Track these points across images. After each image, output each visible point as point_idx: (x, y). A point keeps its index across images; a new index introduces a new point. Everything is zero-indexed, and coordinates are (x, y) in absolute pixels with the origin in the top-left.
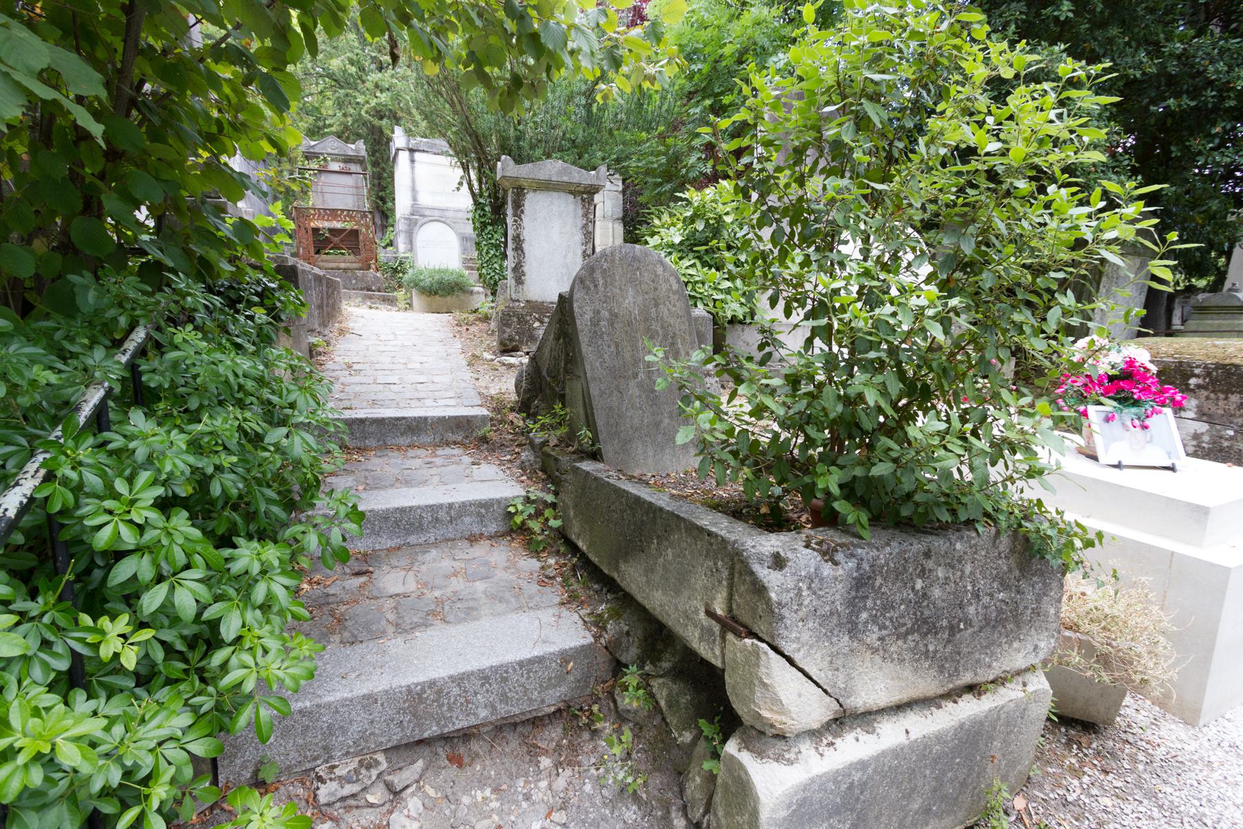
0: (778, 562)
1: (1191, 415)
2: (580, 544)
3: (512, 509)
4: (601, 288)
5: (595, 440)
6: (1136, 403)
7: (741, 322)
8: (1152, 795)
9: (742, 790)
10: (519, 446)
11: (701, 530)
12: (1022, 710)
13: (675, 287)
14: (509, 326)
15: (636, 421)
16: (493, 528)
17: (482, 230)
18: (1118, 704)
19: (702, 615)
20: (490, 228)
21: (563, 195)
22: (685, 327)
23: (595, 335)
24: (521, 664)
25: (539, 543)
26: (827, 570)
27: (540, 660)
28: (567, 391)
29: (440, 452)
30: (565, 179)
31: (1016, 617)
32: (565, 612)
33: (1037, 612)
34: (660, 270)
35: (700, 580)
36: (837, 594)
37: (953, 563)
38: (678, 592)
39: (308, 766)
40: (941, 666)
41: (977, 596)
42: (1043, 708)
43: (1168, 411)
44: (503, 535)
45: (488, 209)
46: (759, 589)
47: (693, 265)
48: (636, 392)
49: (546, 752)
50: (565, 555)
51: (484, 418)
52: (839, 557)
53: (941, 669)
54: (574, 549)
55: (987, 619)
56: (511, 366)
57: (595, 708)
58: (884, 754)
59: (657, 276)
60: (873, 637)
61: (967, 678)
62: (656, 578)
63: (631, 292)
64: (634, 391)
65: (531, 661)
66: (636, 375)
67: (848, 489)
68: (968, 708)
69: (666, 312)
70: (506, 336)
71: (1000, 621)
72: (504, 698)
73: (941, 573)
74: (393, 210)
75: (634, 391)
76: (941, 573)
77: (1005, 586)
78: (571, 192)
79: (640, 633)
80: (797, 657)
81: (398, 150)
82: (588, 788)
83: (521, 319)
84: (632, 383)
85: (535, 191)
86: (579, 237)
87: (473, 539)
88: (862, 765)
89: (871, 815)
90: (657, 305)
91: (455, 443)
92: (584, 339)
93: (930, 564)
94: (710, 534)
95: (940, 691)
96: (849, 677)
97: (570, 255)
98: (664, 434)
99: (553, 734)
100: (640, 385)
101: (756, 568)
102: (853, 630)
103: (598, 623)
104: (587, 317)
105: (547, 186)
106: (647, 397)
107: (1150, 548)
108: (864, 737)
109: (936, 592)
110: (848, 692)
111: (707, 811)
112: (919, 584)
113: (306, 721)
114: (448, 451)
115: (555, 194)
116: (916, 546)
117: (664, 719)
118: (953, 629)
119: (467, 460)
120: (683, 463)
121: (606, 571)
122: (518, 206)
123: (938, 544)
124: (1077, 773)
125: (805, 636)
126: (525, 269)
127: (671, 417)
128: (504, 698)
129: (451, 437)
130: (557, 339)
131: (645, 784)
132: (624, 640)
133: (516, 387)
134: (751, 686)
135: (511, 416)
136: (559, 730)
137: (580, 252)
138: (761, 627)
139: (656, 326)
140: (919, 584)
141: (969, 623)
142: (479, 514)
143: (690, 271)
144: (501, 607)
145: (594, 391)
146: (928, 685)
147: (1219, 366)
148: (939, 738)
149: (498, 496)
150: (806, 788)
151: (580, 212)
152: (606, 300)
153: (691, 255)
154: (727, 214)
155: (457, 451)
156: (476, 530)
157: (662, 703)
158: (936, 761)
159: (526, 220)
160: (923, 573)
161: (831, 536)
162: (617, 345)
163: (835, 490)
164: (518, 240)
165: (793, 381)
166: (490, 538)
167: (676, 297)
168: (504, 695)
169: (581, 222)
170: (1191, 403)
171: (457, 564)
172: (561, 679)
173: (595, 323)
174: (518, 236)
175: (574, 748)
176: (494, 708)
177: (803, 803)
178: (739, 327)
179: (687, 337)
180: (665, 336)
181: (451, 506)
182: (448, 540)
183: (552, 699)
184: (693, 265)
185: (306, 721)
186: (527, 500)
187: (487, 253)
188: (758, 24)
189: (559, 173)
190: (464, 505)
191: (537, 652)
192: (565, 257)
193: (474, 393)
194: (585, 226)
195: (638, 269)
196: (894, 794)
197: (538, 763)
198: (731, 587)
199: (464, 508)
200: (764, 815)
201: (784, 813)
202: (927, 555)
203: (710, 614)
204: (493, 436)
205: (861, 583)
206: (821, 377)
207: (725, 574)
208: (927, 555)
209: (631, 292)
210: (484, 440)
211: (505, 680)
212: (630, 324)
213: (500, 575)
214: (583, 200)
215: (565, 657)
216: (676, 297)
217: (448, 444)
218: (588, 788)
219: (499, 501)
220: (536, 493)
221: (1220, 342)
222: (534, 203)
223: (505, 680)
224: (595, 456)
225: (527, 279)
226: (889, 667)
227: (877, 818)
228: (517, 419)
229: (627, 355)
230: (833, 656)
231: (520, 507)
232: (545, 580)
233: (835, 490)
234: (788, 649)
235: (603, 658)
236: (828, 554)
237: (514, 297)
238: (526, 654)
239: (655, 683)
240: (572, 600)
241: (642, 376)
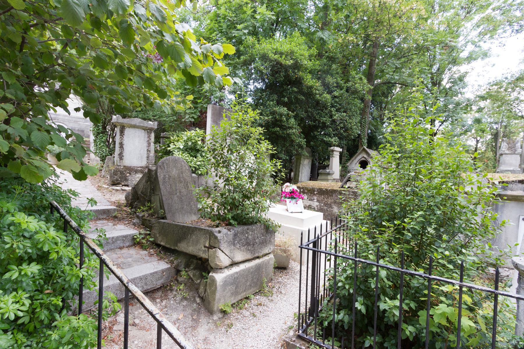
0: (219, 232)
1: (315, 201)
2: (162, 243)
3: (135, 237)
4: (166, 169)
5: (165, 213)
6: (295, 198)
8: (293, 278)
9: (213, 280)
10: (130, 218)
11: (202, 229)
12: (268, 261)
13: (187, 168)
14: (116, 175)
15: (176, 207)
16: (128, 244)
17: (97, 135)
18: (289, 262)
19: (203, 248)
20: (101, 135)
21: (140, 130)
22: (190, 180)
23: (164, 182)
24: (151, 274)
25: (146, 246)
26: (229, 233)
27: (156, 272)
28: (152, 199)
29: (98, 222)
30: (142, 125)
31: (266, 242)
32: (160, 262)
33: (270, 241)
34: (183, 163)
35: (202, 240)
36: (231, 237)
37: (253, 231)
38: (196, 245)
39: (89, 309)
40: (252, 252)
41: (258, 238)
42: (272, 262)
43: (301, 200)
44: (131, 246)
45: (101, 127)
46: (216, 238)
48: (177, 199)
49: (158, 298)
50: (155, 248)
51: (114, 210)
52: (231, 230)
53: (252, 253)
54: (158, 246)
55: (260, 243)
56: (125, 190)
57: (172, 284)
58: (241, 271)
60: (238, 246)
61: (257, 255)
62: (190, 244)
63: (175, 170)
64: (176, 198)
65: (154, 273)
66: (176, 194)
67: (233, 218)
68: (257, 261)
70: (115, 179)
71: (263, 243)
72: (146, 284)
73: (250, 233)
75: (176, 198)
76: (250, 233)
77: (263, 236)
78: (143, 129)
79: (184, 261)
80: (224, 250)
82: (172, 302)
83: (122, 173)
84: (175, 196)
86: (146, 144)
87: (121, 248)
88: (237, 273)
89: (239, 285)
90: (182, 173)
91: (103, 219)
92: (161, 183)
93: (248, 231)
94: (204, 229)
95: (252, 258)
96: (234, 255)
97: (142, 150)
99: (160, 293)
100: (178, 197)
101: (215, 234)
102: (234, 245)
103: (172, 262)
104: (162, 177)
105: (134, 127)
107: (295, 229)
108: (237, 268)
109: (250, 237)
110: (234, 257)
111: (205, 293)
112: (246, 235)
113: (89, 295)
114: (101, 222)
115: (137, 129)
116: (246, 227)
117: (192, 280)
118: (253, 245)
119: (111, 224)
121: (173, 248)
122: (122, 132)
123: (250, 227)
124: (281, 277)
125: (225, 246)
126: (124, 154)
127: (187, 205)
128: (146, 284)
129: (101, 217)
130: (147, 182)
131: (188, 295)
132: (180, 264)
133: (126, 198)
134: (214, 258)
135: (125, 209)
136: (161, 293)
137: (146, 150)
138: (216, 245)
139: (182, 180)
140: (246, 235)
141: (256, 243)
142: (123, 240)
144: (138, 263)
145: (164, 199)
146: (249, 256)
147: (320, 189)
148: (252, 267)
149: (129, 233)
150: (226, 278)
151: (147, 136)
152: (167, 172)
153: (186, 152)
155: (105, 222)
156: (122, 245)
157: (192, 276)
158: (252, 273)
159: (125, 137)
160: (247, 233)
161: (230, 227)
162: (171, 185)
163: (230, 218)
164: (121, 145)
165: (222, 195)
166: (127, 247)
168: (146, 283)
169: (147, 139)
170: (315, 198)
171: (119, 255)
172: (162, 277)
173: (164, 178)
174: (122, 143)
175: (166, 296)
176: (143, 287)
177: (225, 281)
180: (185, 182)
181: (113, 238)
182: (112, 249)
183: (159, 283)
185: (89, 295)
186: (140, 234)
187: (100, 144)
189: (140, 123)
190: (118, 237)
191: (155, 270)
192: (140, 151)
193: (105, 201)
194: (148, 141)
196: (244, 281)
197: (156, 301)
198: (210, 238)
199: (118, 238)
200: (218, 284)
201: (222, 284)
202: (248, 229)
203: (205, 247)
204: (119, 215)
205: (235, 235)
206: (227, 194)
207: (208, 237)
208: (248, 229)
209: (175, 170)
210: (115, 217)
211: (146, 279)
212: (174, 179)
213: (135, 256)
214: (148, 132)
215: (163, 271)
217: (100, 219)
218: (172, 302)
219: (130, 235)
220: (142, 231)
221: (322, 182)
222: (128, 132)
223: (146, 279)
224: (164, 218)
225: (124, 158)
226: (241, 252)
227: (240, 286)
228: (128, 209)
229: (174, 188)
230: (231, 250)
231: (139, 236)
232: (151, 255)
233: (230, 218)
234: (222, 248)
235: (173, 271)
236: (229, 230)
237: (118, 164)
238: (152, 271)
239: (189, 273)
240: (161, 259)
241: (178, 194)
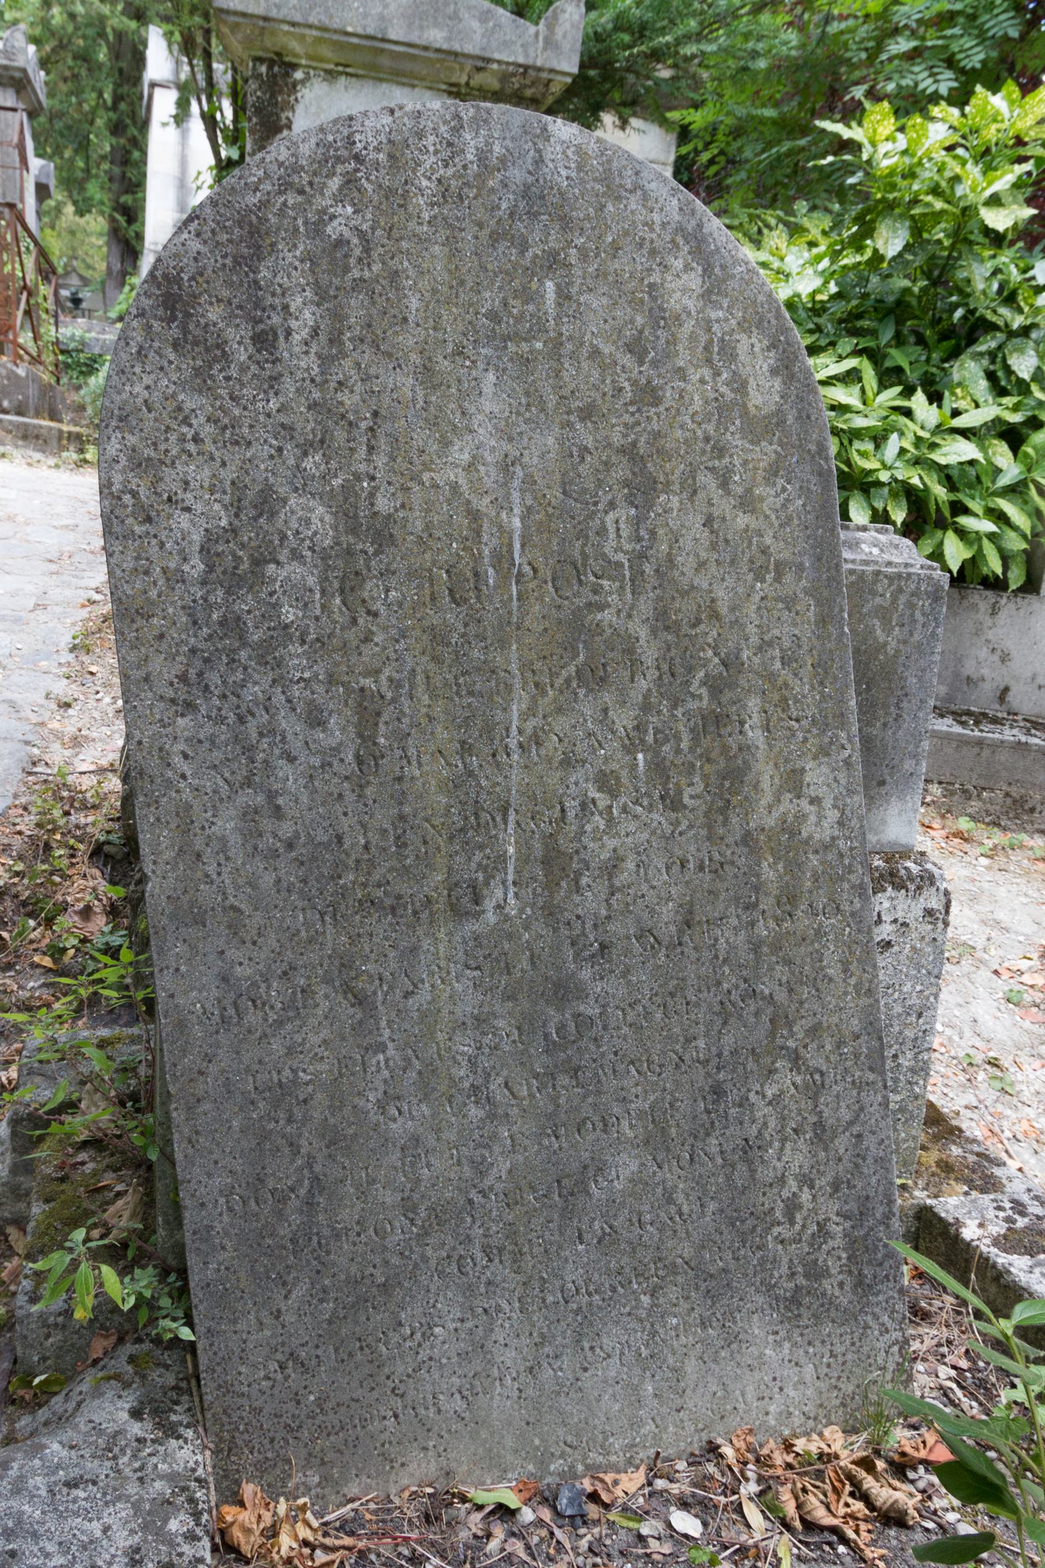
7: (996, 584)
30: (436, 37)
47: (851, 377)
59: (659, 317)
69: (695, 531)
74: (140, 237)
81: (153, 85)
85: (331, 75)
98: (607, 1241)
106: (527, 1026)
120: (697, 1402)
143: (840, 394)
153: (847, 344)
154: (995, 201)
167: (767, 451)
178: (981, 599)
179: (801, 687)
184: (851, 377)
188: (448, 1474)
195: (553, 262)
216: (767, 451)
